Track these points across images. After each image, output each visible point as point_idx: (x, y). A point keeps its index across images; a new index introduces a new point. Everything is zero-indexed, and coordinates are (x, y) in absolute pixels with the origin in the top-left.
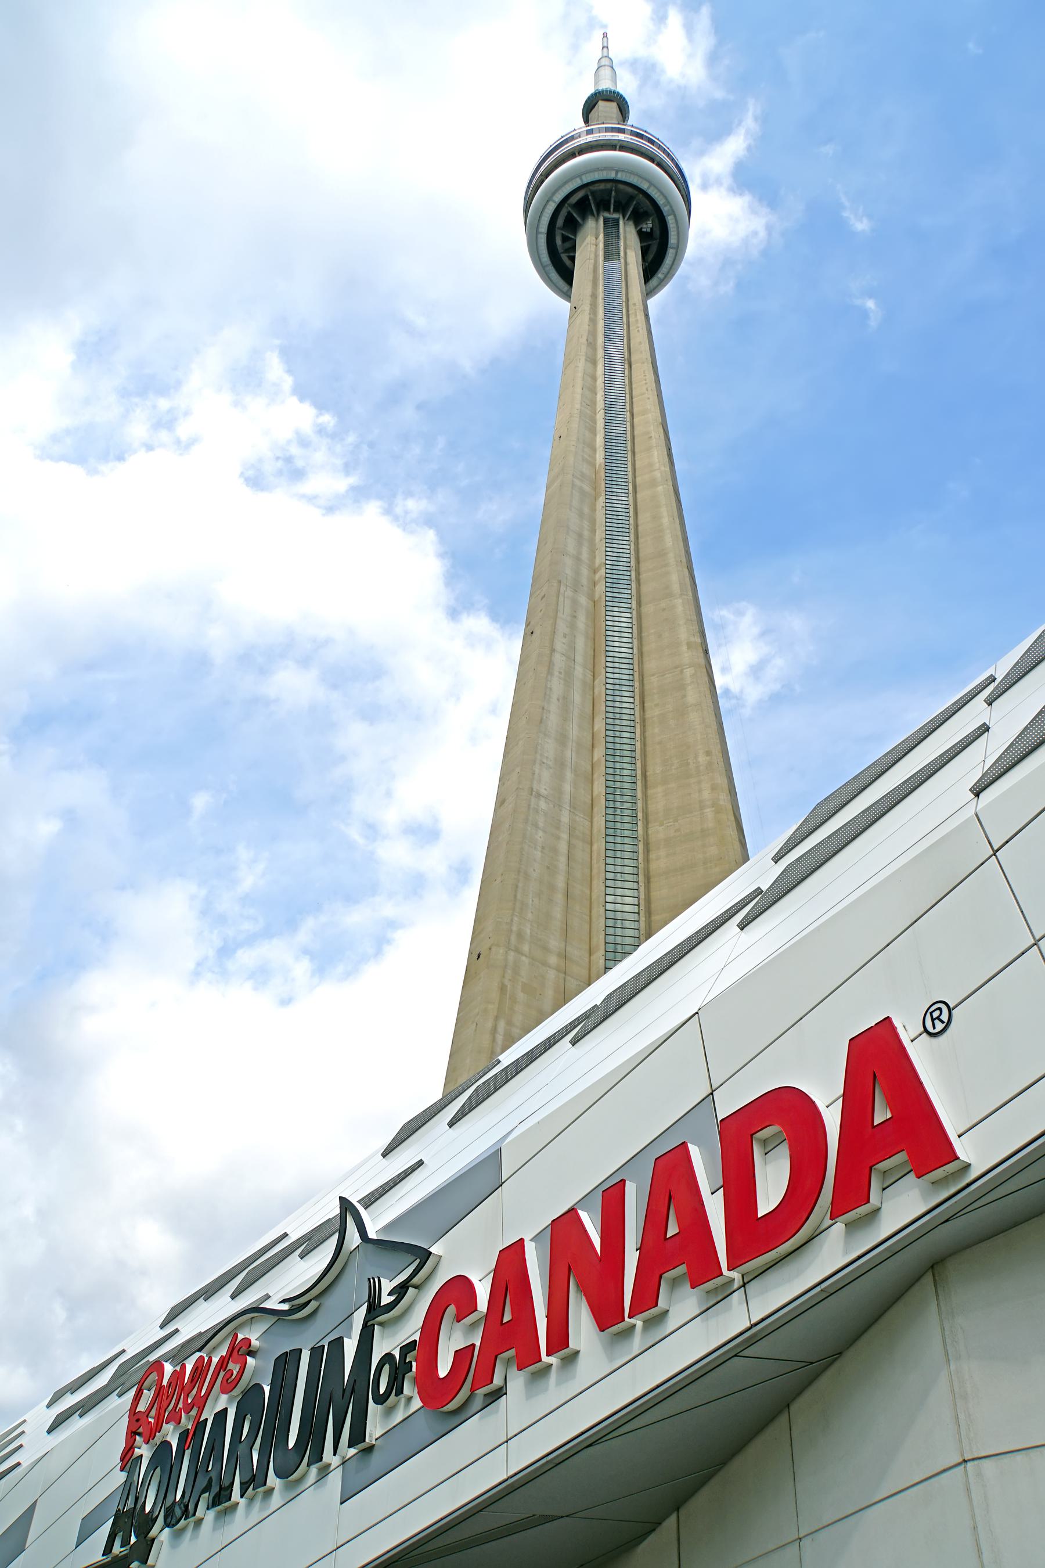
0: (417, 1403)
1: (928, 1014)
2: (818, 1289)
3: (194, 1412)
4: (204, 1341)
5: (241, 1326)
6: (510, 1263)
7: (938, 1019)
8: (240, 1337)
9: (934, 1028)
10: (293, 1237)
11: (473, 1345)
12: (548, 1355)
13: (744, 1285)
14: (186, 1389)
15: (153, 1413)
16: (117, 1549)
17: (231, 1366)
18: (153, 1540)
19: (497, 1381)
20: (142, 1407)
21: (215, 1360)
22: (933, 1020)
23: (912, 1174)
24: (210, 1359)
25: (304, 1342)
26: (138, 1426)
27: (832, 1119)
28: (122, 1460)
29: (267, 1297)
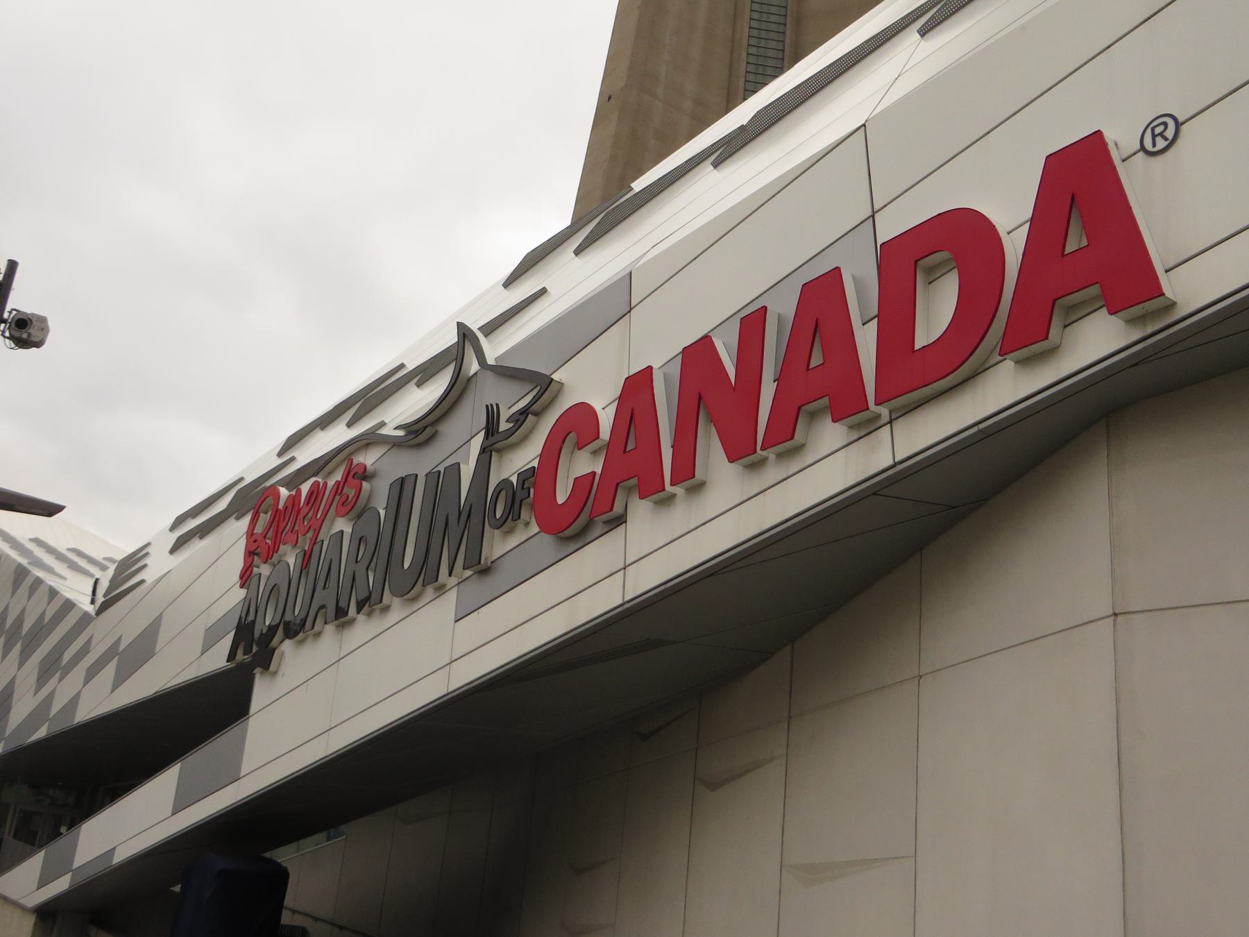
0: (535, 528)
1: (1149, 130)
2: (975, 429)
3: (310, 535)
4: (319, 466)
5: (359, 449)
6: (638, 387)
7: (1163, 135)
8: (355, 462)
9: (1154, 145)
10: (410, 366)
11: (594, 473)
12: (672, 484)
13: (890, 422)
14: (303, 513)
15: (270, 534)
16: (240, 656)
17: (346, 490)
18: (274, 650)
19: (618, 508)
20: (259, 529)
21: (331, 483)
22: (1154, 136)
23: (1104, 310)
24: (326, 484)
25: (421, 464)
26: (257, 551)
27: (1014, 246)
28: (241, 578)
29: (382, 424)
